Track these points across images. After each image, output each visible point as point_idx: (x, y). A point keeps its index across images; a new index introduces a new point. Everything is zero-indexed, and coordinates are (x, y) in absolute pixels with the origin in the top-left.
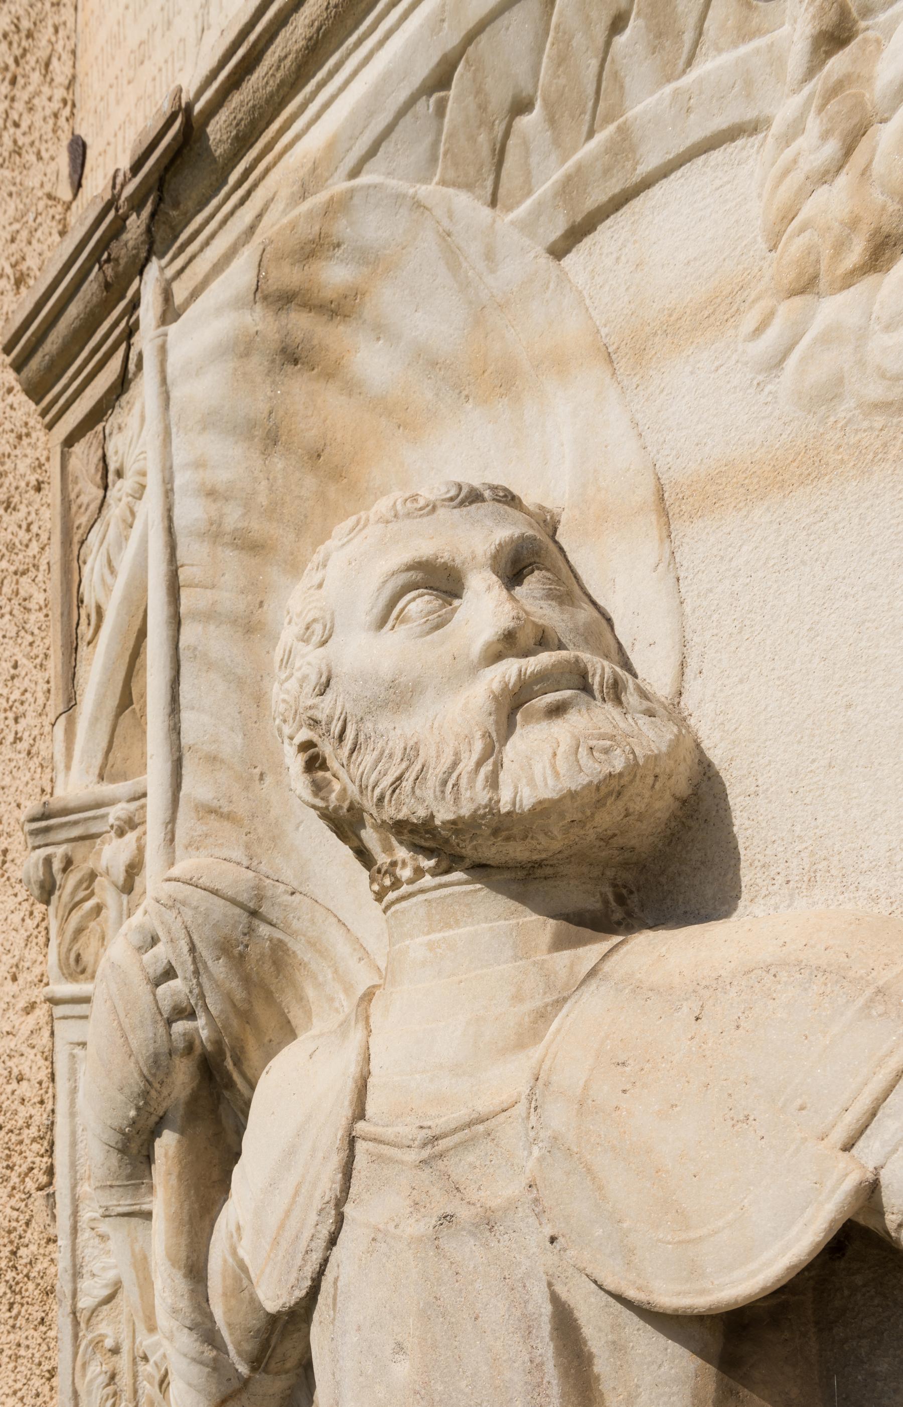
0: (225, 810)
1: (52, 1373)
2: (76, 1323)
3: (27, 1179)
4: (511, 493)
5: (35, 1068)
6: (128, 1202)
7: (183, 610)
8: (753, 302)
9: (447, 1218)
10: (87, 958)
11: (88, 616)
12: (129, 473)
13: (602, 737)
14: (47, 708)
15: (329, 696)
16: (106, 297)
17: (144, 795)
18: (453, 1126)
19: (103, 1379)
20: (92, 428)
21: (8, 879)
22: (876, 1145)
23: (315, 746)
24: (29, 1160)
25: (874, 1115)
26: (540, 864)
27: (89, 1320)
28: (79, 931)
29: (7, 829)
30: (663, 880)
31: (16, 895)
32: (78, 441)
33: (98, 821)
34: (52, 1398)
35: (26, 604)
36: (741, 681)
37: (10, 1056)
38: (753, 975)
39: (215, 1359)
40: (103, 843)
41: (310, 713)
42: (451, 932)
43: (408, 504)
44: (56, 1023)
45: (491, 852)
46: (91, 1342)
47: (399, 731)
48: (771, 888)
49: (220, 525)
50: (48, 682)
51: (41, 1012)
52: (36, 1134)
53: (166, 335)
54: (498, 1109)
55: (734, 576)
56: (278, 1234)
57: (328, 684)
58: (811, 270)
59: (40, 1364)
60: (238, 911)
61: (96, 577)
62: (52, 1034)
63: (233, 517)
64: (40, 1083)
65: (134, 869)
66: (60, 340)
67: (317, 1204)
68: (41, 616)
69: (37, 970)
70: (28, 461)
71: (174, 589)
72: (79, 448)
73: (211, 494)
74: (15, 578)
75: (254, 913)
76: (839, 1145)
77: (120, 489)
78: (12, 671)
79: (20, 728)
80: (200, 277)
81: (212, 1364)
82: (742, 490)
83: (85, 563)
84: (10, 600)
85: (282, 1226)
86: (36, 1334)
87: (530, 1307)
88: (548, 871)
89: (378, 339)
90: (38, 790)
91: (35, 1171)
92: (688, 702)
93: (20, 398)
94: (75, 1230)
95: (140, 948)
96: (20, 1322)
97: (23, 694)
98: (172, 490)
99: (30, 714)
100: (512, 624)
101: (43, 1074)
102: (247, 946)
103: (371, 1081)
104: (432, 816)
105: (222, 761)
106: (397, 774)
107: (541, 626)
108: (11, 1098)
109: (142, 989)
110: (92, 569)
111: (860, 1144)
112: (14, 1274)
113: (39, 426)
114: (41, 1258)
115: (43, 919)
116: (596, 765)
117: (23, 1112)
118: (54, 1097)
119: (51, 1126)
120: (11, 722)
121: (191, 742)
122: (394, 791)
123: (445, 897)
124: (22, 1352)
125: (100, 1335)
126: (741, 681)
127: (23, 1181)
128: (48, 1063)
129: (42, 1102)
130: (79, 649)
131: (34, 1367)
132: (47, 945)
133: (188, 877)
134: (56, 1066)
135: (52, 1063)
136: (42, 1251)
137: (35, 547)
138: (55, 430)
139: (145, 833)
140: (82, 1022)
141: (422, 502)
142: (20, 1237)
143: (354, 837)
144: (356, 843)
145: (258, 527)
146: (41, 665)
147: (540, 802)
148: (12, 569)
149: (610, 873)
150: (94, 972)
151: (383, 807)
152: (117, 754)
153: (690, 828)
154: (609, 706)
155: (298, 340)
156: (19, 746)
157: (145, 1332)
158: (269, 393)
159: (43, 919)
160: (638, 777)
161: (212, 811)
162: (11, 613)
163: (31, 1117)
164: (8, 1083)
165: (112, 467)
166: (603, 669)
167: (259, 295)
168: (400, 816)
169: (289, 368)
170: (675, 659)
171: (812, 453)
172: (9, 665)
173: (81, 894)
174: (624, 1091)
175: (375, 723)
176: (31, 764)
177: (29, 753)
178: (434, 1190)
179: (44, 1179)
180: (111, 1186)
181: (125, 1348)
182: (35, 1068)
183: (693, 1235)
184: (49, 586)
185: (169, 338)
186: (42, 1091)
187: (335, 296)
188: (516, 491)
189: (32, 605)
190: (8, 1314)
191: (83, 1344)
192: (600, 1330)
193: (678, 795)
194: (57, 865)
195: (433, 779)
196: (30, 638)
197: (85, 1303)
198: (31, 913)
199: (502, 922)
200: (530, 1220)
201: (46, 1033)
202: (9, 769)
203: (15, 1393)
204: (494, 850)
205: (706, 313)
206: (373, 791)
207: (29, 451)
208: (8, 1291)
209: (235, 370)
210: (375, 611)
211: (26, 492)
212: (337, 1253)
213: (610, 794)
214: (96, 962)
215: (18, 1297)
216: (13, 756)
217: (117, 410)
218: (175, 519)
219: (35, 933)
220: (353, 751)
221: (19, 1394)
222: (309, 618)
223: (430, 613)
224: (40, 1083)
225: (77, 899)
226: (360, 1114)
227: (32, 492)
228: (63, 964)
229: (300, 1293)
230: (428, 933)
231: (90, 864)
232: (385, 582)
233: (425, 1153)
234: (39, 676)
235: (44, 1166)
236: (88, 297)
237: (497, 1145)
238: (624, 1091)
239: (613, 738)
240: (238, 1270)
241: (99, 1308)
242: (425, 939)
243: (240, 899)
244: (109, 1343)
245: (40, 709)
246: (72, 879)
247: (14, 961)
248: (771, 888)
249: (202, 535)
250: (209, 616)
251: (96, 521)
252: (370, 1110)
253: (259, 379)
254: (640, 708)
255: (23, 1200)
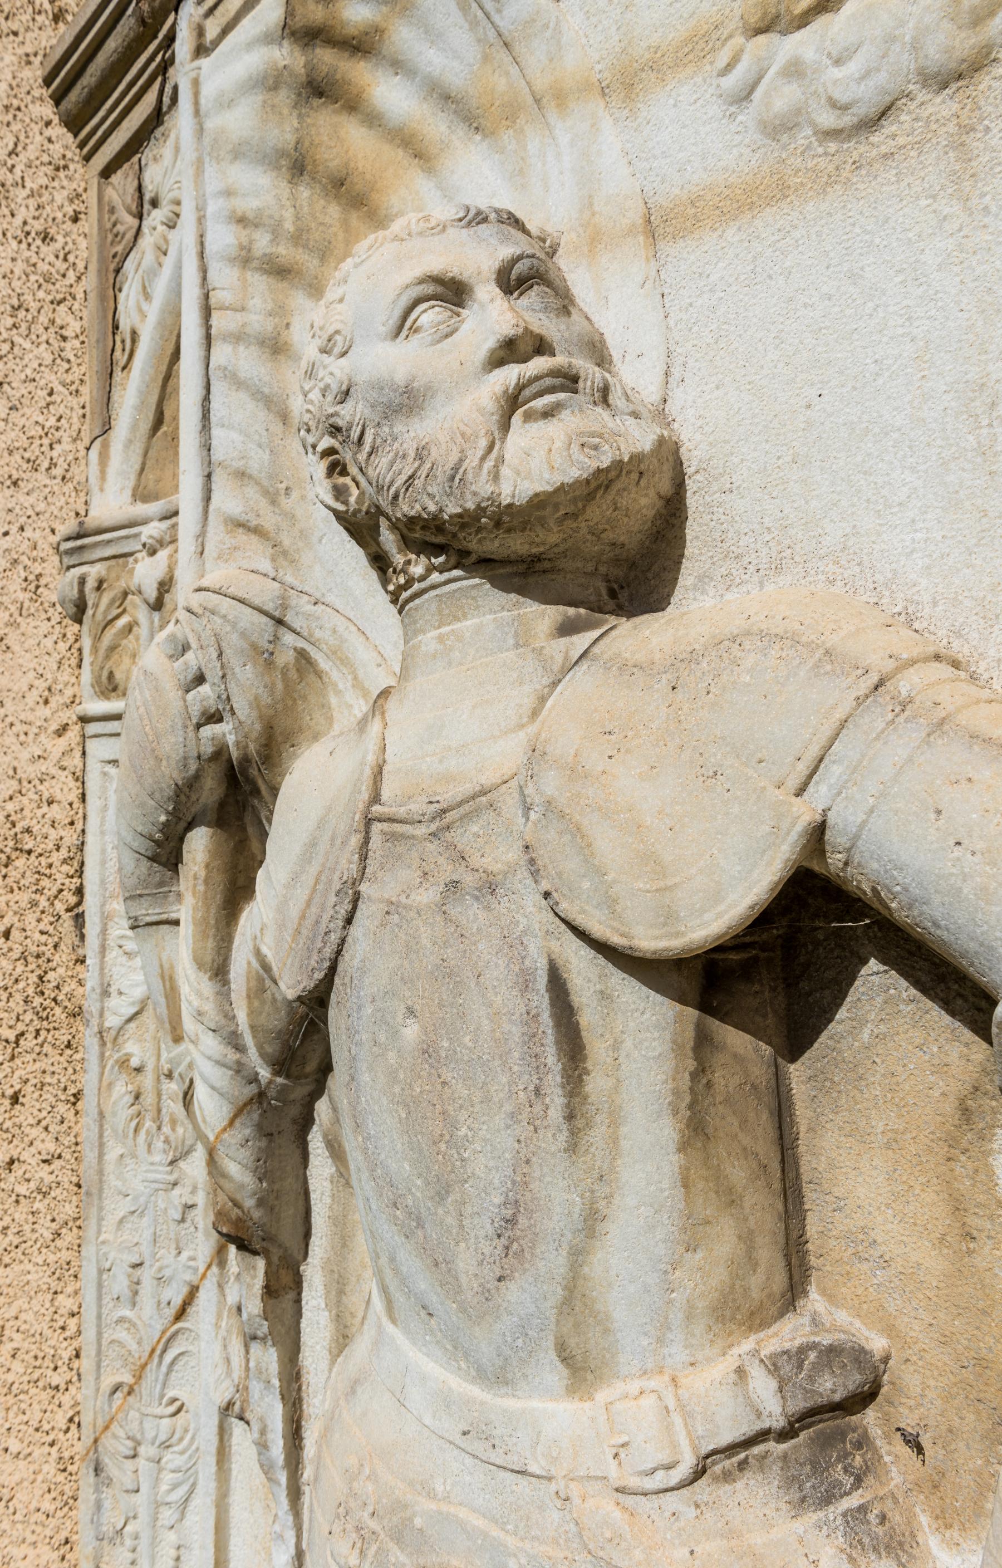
0: (254, 523)
1: (77, 1096)
2: (103, 1043)
3: (56, 902)
4: (514, 216)
5: (66, 790)
6: (157, 911)
7: (213, 331)
8: (726, 40)
9: (455, 884)
10: (119, 676)
11: (123, 341)
12: (164, 202)
13: (593, 435)
14: (83, 433)
15: (349, 404)
16: (143, 33)
17: (176, 513)
18: (459, 799)
19: (129, 1099)
20: (128, 160)
21: (42, 603)
22: (823, 789)
23: (336, 452)
24: (59, 882)
25: (821, 760)
26: (538, 558)
27: (115, 1039)
28: (112, 648)
29: (42, 555)
30: (650, 575)
31: (49, 619)
32: (115, 172)
33: (131, 540)
34: (76, 1123)
35: (64, 332)
36: (717, 388)
37: (41, 781)
38: (722, 646)
39: (239, 1063)
40: (136, 561)
41: (332, 421)
42: (459, 625)
43: (421, 223)
44: (88, 742)
45: (493, 546)
46: (117, 1061)
47: (412, 434)
48: (744, 577)
49: (249, 251)
50: (83, 407)
51: (73, 735)
52: (66, 855)
53: (200, 68)
54: (500, 781)
55: (711, 290)
56: (300, 924)
57: (347, 392)
58: (774, 11)
59: (65, 1089)
60: (265, 619)
61: (132, 302)
62: (84, 753)
63: (262, 242)
64: (71, 804)
65: (165, 586)
66: (99, 73)
67: (337, 885)
68: (77, 343)
69: (69, 692)
70: (65, 193)
71: (207, 311)
72: (116, 178)
73: (242, 221)
74: (52, 307)
75: (280, 622)
76: (793, 791)
77: (155, 217)
78: (48, 399)
79: (55, 454)
80: (232, 13)
81: (235, 1067)
82: (717, 212)
83: (120, 290)
84: (46, 329)
85: (303, 917)
86: (62, 1059)
87: (527, 962)
88: (547, 565)
89: (397, 74)
90: (73, 514)
91: (65, 893)
92: (672, 408)
93: (58, 131)
94: (103, 949)
95: (171, 657)
96: (47, 1048)
97: (59, 420)
98: (204, 216)
99: (66, 439)
100: (512, 332)
101: (74, 796)
102: (272, 654)
103: (386, 769)
104: (441, 510)
105: (250, 477)
106: (410, 473)
107: (538, 335)
108: (42, 822)
109: (173, 694)
110: (128, 296)
111: (811, 788)
112: (41, 1000)
113: (76, 158)
114: (68, 980)
115: (76, 640)
116: (587, 460)
117: (53, 835)
118: (84, 818)
119: (81, 847)
120: (46, 448)
121: (221, 459)
122: (407, 490)
123: (455, 591)
124: (48, 1079)
125: (126, 1054)
126: (717, 388)
127: (52, 904)
128: (79, 784)
129: (72, 823)
130: (114, 375)
131: (60, 1093)
132: (80, 667)
133: (217, 587)
134: (89, 785)
135: (83, 783)
136: (70, 973)
137: (71, 275)
138: (92, 161)
139: (176, 551)
140: (113, 739)
141: (433, 223)
142: (49, 961)
143: (373, 543)
144: (374, 549)
145: (284, 251)
146: (77, 391)
147: (537, 495)
148: (50, 298)
149: (603, 569)
150: (126, 689)
151: (397, 505)
152: (150, 476)
153: (673, 526)
154: (599, 410)
155: (323, 74)
156: (54, 472)
157: (171, 1043)
158: (296, 125)
159: (76, 640)
160: (624, 472)
161: (240, 525)
162: (47, 342)
163: (61, 838)
164: (39, 807)
165: (147, 197)
166: (594, 374)
167: (287, 31)
168: (412, 513)
169: (316, 102)
170: (661, 368)
171: (776, 177)
172: (45, 392)
173: (116, 612)
174: (610, 757)
175: (391, 427)
176: (65, 489)
177: (64, 478)
178: (441, 860)
179: (73, 900)
180: (140, 896)
181: (150, 1067)
182: (66, 790)
183: (669, 882)
184: (85, 314)
185: (203, 72)
186: (73, 812)
187: (356, 33)
188: (519, 215)
189: (68, 333)
190: (35, 1042)
191: (110, 1063)
192: (589, 981)
193: (662, 493)
194: (90, 584)
195: (441, 475)
196: (66, 366)
197: (112, 1021)
198: (64, 635)
199: (505, 613)
200: (528, 882)
201: (78, 754)
202: (43, 494)
203: (39, 1121)
204: (496, 543)
205: (686, 50)
206: (388, 490)
207: (65, 183)
208: (35, 1018)
209: (265, 102)
210: (391, 322)
211: (64, 222)
212: (356, 931)
213: (599, 487)
214: (128, 678)
215: (45, 1023)
216: (48, 482)
217: (153, 141)
218: (207, 244)
219: (68, 654)
220: (370, 454)
221: (44, 1123)
222: (331, 330)
223: (440, 323)
224: (71, 804)
225: (110, 617)
226: (376, 798)
227: (69, 223)
228: (97, 682)
229: (319, 975)
230: (439, 627)
231: (122, 584)
232: (399, 295)
233: (433, 827)
234: (74, 402)
235: (73, 887)
236: (126, 31)
237: (499, 815)
238: (610, 757)
239: (600, 436)
240: (261, 971)
241: (127, 1027)
242: (435, 633)
243: (265, 608)
244: (134, 1062)
245: (74, 434)
246: (106, 599)
247: (46, 685)
248: (744, 577)
249: (232, 260)
250: (238, 338)
251: (131, 249)
252: (386, 794)
253: (286, 111)
254: (627, 411)
255: (51, 924)
